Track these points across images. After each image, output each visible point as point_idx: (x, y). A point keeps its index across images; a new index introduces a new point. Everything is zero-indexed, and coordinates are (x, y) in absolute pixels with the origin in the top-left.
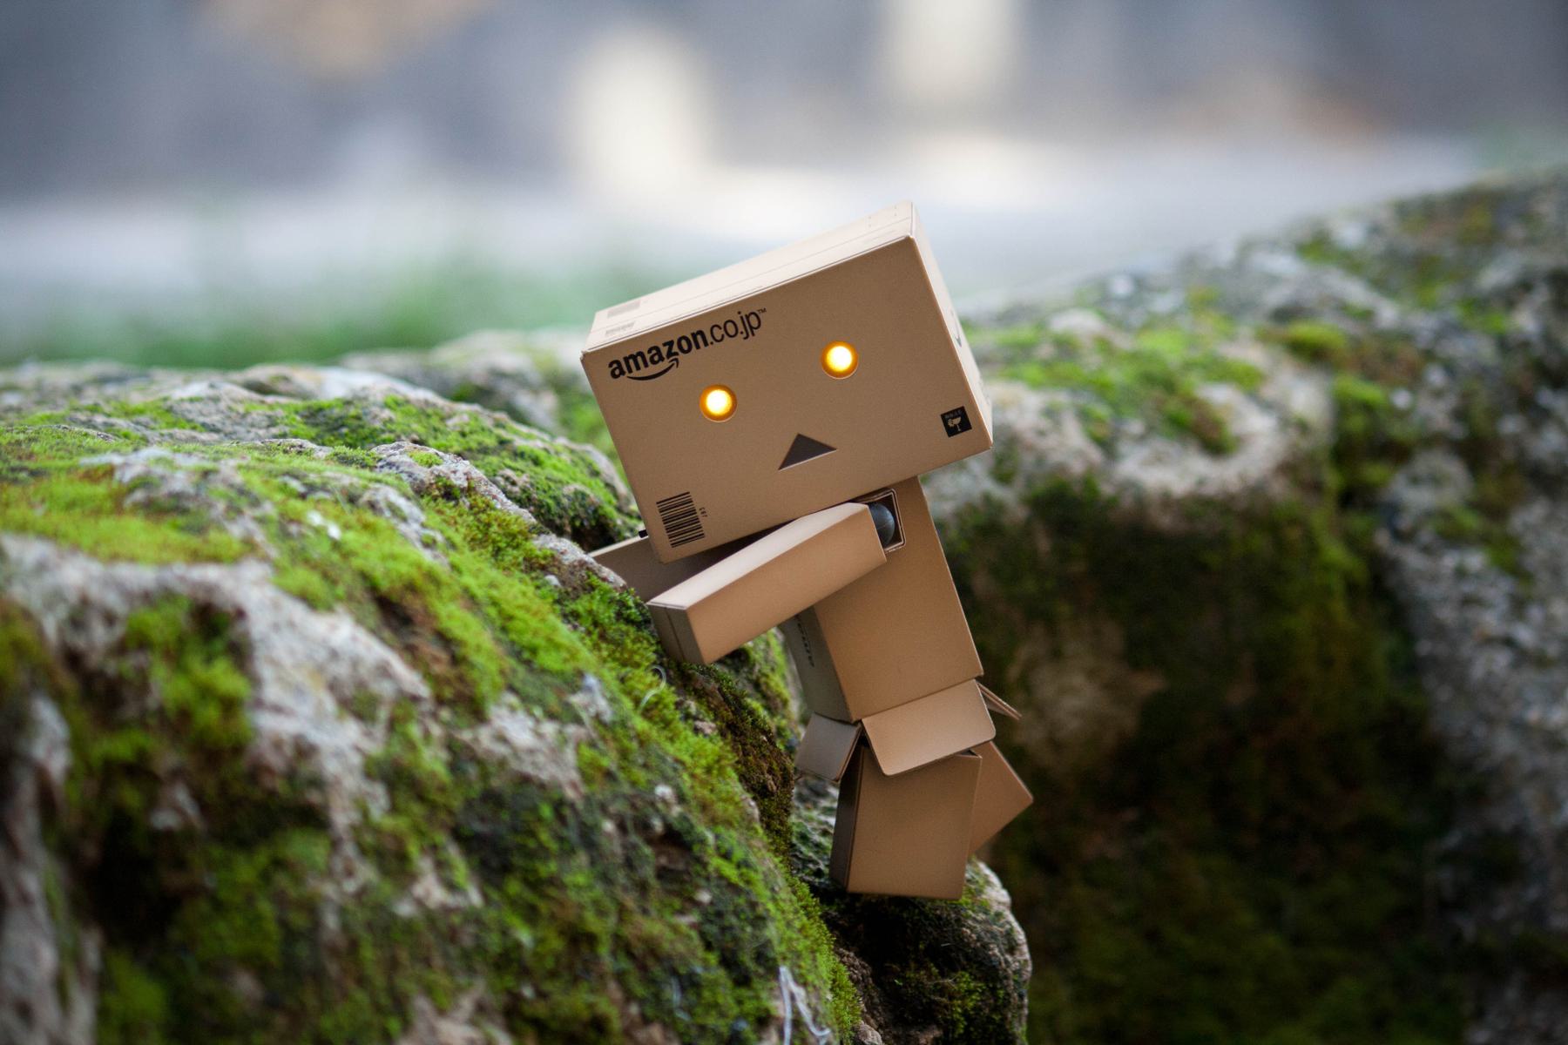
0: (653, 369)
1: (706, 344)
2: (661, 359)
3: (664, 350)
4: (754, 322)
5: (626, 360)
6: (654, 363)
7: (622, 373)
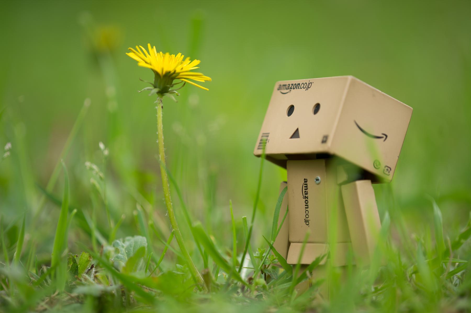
0: (304, 191)
3: (306, 196)
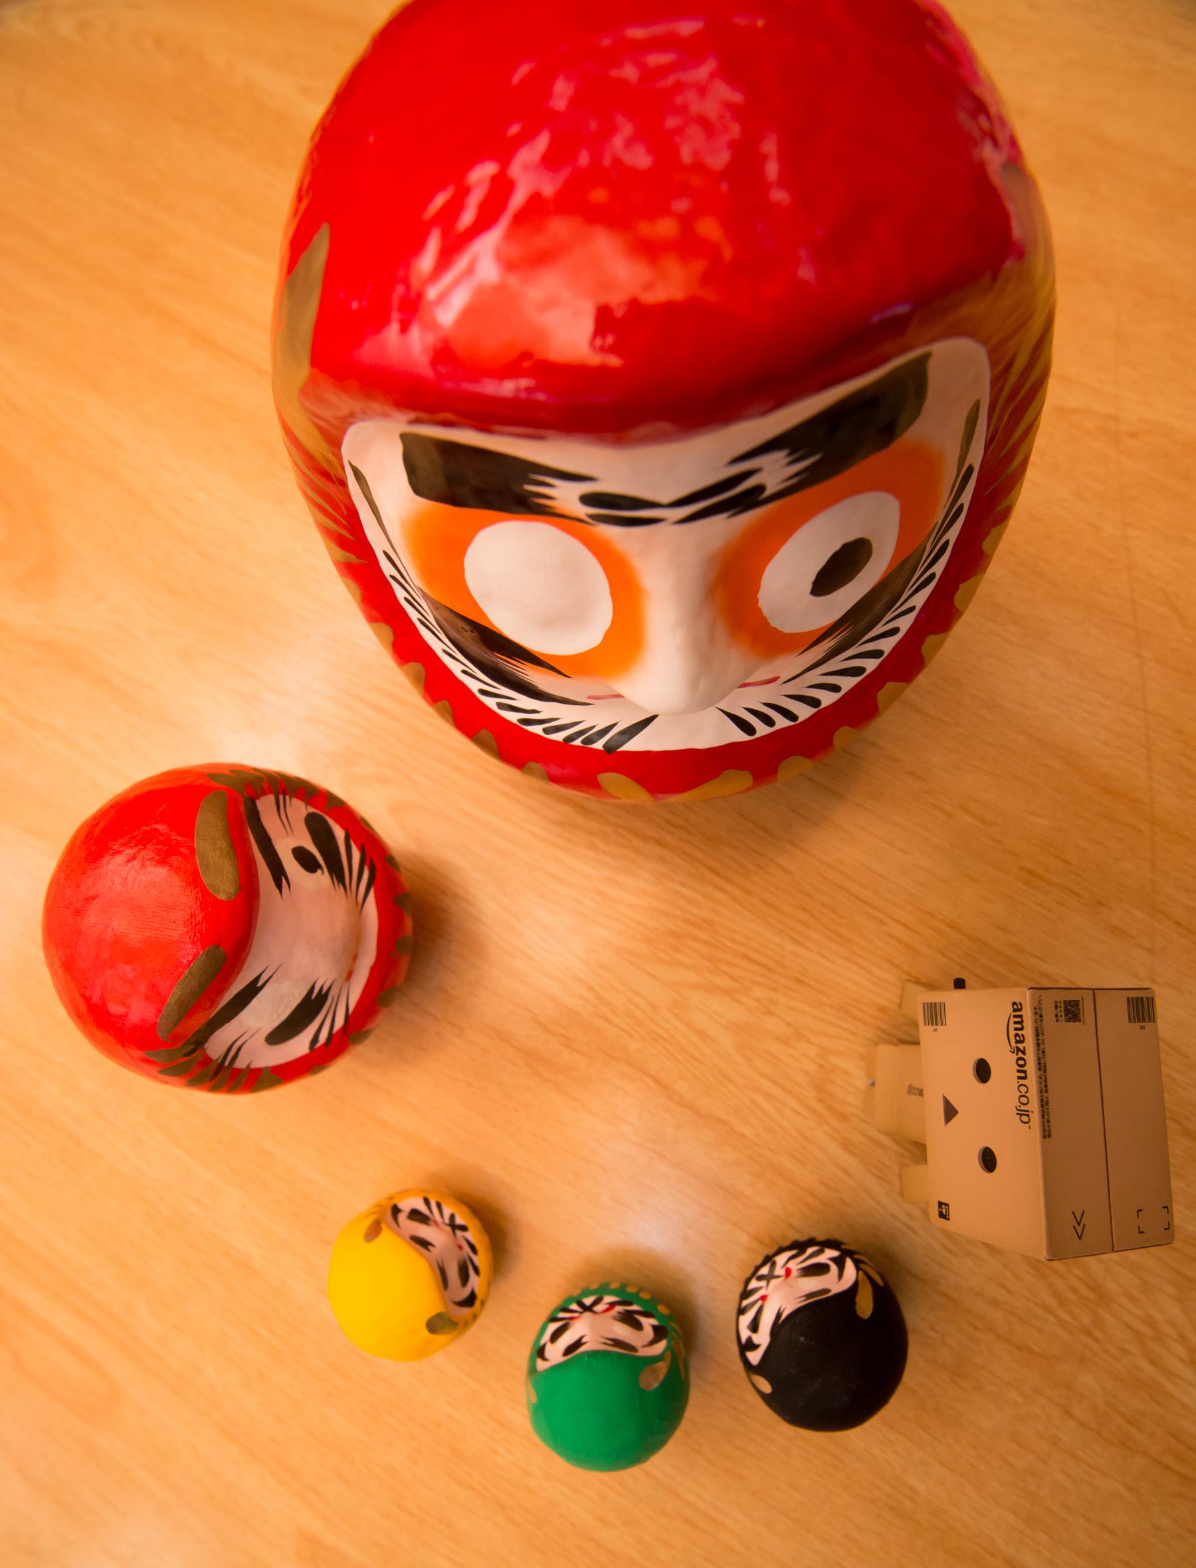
1: (1019, 1078)
2: (1017, 1042)
4: (1025, 1119)
5: (1021, 1016)
6: (1017, 1035)
7: (1015, 1010)
